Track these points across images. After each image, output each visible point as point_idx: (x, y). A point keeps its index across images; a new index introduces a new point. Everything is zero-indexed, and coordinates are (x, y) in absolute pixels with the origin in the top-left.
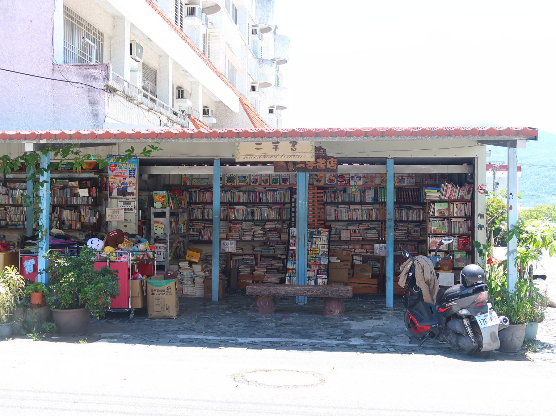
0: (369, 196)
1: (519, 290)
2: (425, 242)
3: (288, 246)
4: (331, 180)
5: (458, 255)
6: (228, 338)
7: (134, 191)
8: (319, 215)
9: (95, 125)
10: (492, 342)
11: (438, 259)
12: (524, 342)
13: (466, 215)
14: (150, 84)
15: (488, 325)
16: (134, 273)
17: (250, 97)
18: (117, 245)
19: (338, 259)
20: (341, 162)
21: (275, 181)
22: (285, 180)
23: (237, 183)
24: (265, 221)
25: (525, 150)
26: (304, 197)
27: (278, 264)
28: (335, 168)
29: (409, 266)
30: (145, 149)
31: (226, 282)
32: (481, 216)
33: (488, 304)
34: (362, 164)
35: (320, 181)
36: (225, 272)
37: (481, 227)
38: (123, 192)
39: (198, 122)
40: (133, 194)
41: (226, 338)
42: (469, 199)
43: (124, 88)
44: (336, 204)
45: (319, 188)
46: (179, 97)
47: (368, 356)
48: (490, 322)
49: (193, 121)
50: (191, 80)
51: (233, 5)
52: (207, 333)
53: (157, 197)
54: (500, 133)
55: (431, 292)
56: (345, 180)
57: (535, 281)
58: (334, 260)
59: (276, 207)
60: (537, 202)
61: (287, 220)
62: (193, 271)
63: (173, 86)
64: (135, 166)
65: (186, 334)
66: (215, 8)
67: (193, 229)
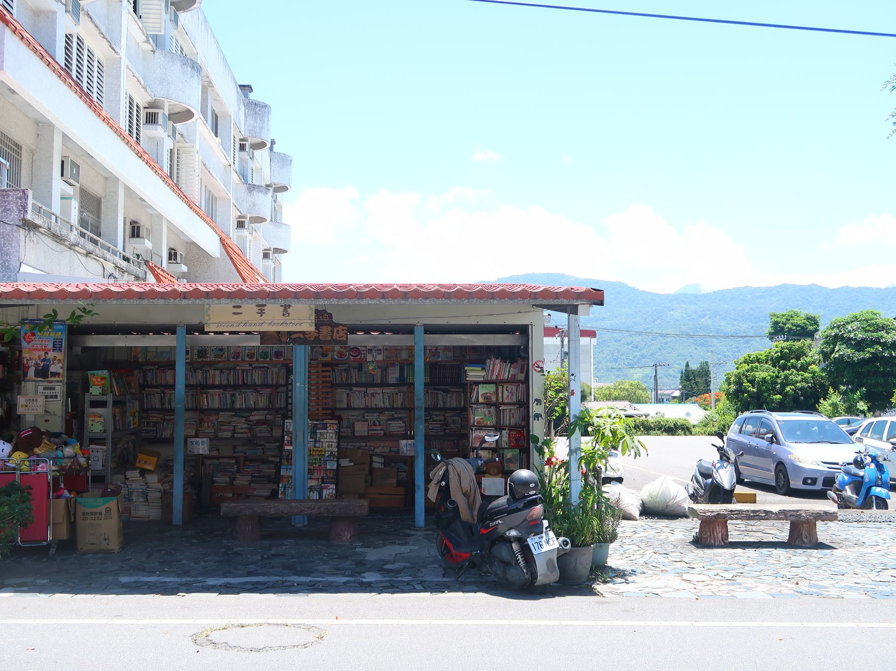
0: (393, 375)
1: (584, 501)
2: (466, 436)
3: (282, 444)
4: (341, 354)
5: (509, 454)
6: (192, 579)
7: (61, 371)
8: (324, 401)
9: (4, 276)
10: (548, 573)
11: (480, 462)
12: (591, 569)
13: (519, 401)
14: (90, 218)
15: (543, 550)
16: (56, 488)
17: (234, 234)
18: (32, 450)
19: (351, 461)
20: (353, 330)
21: (265, 355)
22: (278, 354)
23: (211, 357)
24: (250, 410)
25: (589, 316)
26: (303, 378)
27: (269, 470)
28: (344, 338)
29: (441, 472)
30: (74, 313)
31: (195, 497)
32: (538, 401)
33: (544, 521)
34: (382, 333)
35: (326, 355)
36: (194, 482)
37: (537, 416)
38: (43, 372)
39: (159, 271)
40: (58, 374)
41: (189, 579)
42: (522, 379)
43: (50, 223)
44: (349, 386)
45: (325, 364)
46: (133, 236)
47: (386, 597)
48: (547, 544)
49: (152, 270)
50: (151, 212)
51: (213, 111)
52: (163, 573)
53: (95, 379)
54: (557, 295)
55: (471, 507)
56: (360, 353)
57: (605, 488)
58: (345, 462)
59: (267, 391)
60: (618, 377)
61: (281, 409)
62: (147, 483)
63: (125, 218)
64: (63, 336)
65: (131, 575)
66: (187, 115)
67: (148, 423)
